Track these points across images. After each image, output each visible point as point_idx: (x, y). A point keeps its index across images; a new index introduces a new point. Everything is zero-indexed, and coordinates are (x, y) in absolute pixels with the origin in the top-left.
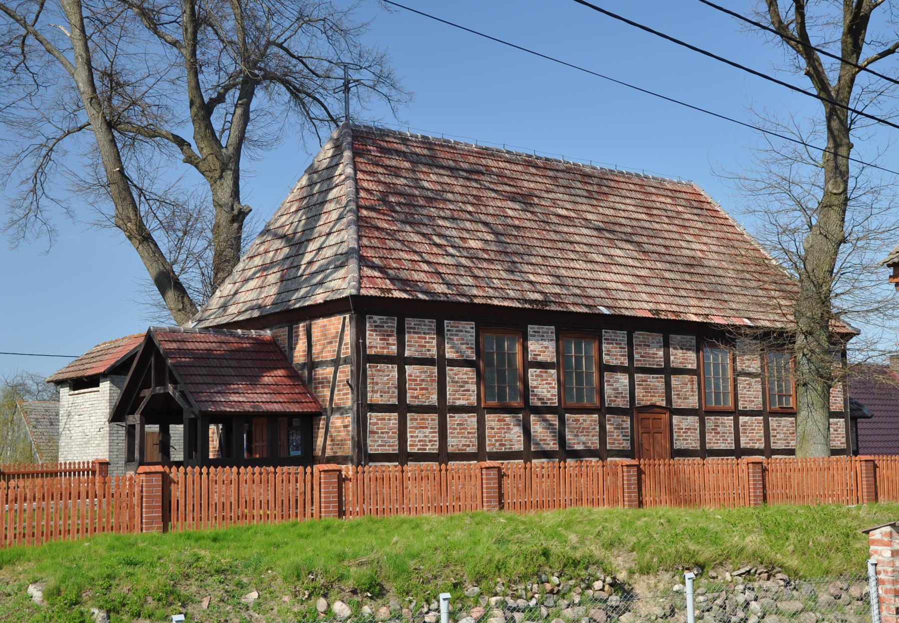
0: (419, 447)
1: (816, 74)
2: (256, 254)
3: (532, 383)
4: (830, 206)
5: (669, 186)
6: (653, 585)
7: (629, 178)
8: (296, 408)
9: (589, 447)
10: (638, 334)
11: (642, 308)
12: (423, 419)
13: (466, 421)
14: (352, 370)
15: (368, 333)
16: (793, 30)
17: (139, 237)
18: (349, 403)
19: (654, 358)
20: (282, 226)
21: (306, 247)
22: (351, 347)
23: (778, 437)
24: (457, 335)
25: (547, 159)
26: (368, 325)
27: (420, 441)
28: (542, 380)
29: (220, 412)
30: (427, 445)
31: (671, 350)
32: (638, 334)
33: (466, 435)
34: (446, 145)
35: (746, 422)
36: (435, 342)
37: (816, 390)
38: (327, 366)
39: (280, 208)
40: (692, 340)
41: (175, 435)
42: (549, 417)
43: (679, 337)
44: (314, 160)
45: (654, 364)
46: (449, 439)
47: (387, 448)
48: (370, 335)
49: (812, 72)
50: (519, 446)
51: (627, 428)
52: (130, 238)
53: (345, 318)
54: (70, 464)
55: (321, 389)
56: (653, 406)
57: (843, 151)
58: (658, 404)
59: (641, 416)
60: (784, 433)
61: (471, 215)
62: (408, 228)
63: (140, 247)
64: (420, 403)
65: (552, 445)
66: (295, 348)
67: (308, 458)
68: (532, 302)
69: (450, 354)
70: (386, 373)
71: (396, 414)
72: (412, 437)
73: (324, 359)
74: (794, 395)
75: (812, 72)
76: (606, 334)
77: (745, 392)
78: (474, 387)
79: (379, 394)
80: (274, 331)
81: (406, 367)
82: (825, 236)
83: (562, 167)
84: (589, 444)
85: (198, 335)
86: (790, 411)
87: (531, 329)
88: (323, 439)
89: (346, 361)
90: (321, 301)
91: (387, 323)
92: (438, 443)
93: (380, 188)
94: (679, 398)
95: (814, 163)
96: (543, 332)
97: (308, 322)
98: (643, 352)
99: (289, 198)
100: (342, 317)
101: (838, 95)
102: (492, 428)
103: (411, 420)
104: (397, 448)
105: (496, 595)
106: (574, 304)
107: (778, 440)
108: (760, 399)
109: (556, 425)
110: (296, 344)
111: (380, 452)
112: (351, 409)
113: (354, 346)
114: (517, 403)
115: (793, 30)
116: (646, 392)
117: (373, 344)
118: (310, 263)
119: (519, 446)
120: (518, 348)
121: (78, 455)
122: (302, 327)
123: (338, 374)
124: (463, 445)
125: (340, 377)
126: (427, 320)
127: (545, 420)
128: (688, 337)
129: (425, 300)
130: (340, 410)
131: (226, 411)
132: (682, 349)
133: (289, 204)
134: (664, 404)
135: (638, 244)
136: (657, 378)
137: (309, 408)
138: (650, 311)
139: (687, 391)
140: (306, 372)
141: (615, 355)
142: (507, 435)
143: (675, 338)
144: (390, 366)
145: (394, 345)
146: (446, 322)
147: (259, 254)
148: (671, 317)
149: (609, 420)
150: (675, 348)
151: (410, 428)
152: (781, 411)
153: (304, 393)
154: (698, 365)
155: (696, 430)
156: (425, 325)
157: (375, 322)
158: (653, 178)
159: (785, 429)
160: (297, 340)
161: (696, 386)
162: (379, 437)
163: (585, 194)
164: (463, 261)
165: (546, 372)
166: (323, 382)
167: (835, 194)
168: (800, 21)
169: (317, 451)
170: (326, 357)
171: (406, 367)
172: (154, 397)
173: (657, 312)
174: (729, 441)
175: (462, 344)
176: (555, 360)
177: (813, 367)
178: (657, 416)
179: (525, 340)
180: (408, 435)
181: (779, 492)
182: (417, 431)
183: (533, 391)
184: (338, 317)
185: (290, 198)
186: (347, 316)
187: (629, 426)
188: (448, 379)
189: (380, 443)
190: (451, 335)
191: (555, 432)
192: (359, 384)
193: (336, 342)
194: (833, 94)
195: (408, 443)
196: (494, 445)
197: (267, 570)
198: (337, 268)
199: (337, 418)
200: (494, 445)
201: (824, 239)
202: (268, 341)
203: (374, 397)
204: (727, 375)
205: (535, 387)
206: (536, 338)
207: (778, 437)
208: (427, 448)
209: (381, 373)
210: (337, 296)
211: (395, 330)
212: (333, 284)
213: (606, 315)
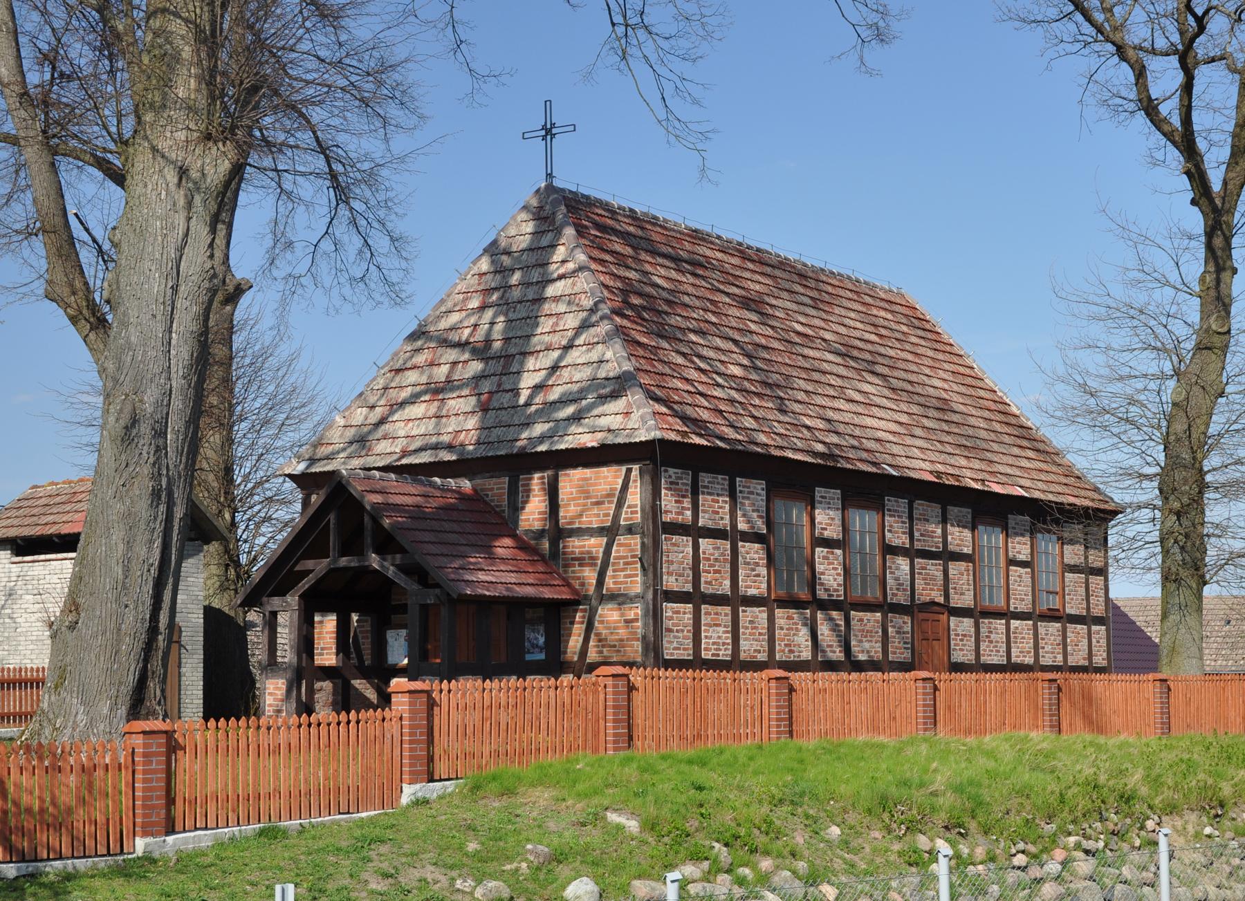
0: (713, 652)
1: (1197, 176)
2: (409, 365)
3: (819, 568)
4: (1209, 349)
5: (883, 295)
6: (1180, 828)
7: (841, 281)
8: (547, 593)
9: (872, 657)
10: (919, 504)
11: (921, 467)
12: (717, 614)
13: (757, 617)
14: (643, 544)
15: (663, 492)
16: (1170, 110)
17: (92, 320)
18: (638, 589)
19: (933, 537)
20: (453, 329)
21: (522, 363)
22: (643, 510)
23: (1046, 649)
24: (748, 498)
25: (758, 250)
26: (663, 480)
27: (714, 643)
28: (829, 564)
29: (476, 595)
30: (720, 650)
31: (949, 526)
32: (919, 504)
33: (757, 637)
34: (654, 221)
35: (1017, 628)
36: (727, 506)
37: (1191, 588)
38: (592, 536)
39: (442, 301)
40: (967, 512)
41: (188, 629)
42: (835, 614)
43: (956, 509)
44: (499, 234)
45: (932, 547)
46: (741, 642)
47: (682, 652)
48: (666, 495)
49: (1193, 170)
50: (806, 655)
51: (908, 633)
52: (74, 320)
53: (629, 471)
54: (38, 670)
55: (577, 568)
56: (933, 603)
57: (1225, 276)
58: (936, 600)
59: (921, 616)
60: (1052, 644)
61: (776, 332)
62: (665, 345)
63: (92, 336)
64: (714, 592)
65: (837, 655)
66: (523, 508)
67: (554, 665)
68: (816, 454)
69: (742, 526)
70: (681, 549)
71: (691, 605)
72: (706, 637)
73: (583, 526)
74: (1061, 593)
75: (1193, 170)
76: (890, 502)
77: (1016, 587)
78: (764, 571)
79: (674, 578)
80: (479, 481)
81: (700, 540)
82: (1203, 388)
83: (774, 261)
84: (872, 654)
85: (395, 483)
86: (1057, 614)
87: (819, 492)
88: (581, 639)
89: (630, 530)
90: (595, 444)
91: (681, 479)
92: (730, 647)
93: (619, 285)
94: (956, 593)
95: (1185, 289)
96: (830, 498)
97: (550, 472)
98: (922, 528)
99: (459, 287)
100: (624, 469)
101: (1223, 203)
102: (782, 628)
103: (706, 614)
104: (691, 652)
105: (1070, 834)
106: (861, 460)
107: (1046, 652)
108: (1030, 597)
109: (841, 625)
110: (526, 502)
111: (675, 657)
112: (642, 597)
113: (648, 508)
114: (804, 595)
115: (1170, 110)
116: (926, 584)
117: (669, 508)
118: (538, 388)
119: (806, 655)
120: (805, 519)
121: (33, 657)
122: (537, 481)
123: (615, 548)
124: (755, 651)
125: (618, 551)
126: (720, 477)
127: (831, 619)
128: (965, 510)
129: (725, 449)
130: (619, 598)
131: (485, 595)
132: (959, 526)
133: (461, 296)
134: (941, 600)
135: (884, 377)
136: (936, 565)
137: (565, 595)
138: (931, 472)
139: (963, 584)
140: (546, 545)
141: (897, 532)
142: (796, 638)
143: (953, 511)
144: (685, 538)
145: (688, 509)
146: (738, 479)
147: (414, 367)
148: (952, 482)
149: (892, 621)
150: (952, 525)
151: (705, 625)
152: (1049, 613)
153: (551, 573)
154: (974, 549)
155: (971, 636)
156: (718, 483)
157: (670, 477)
158: (866, 283)
159: (1052, 638)
160: (528, 496)
161: (971, 578)
162: (675, 637)
163: (809, 301)
164: (733, 393)
165: (833, 553)
166: (585, 560)
167: (1219, 333)
168: (1186, 104)
169: (569, 655)
170: (591, 522)
171: (700, 540)
172: (332, 572)
173: (938, 474)
174: (1001, 653)
175: (753, 511)
176: (841, 537)
177: (1187, 558)
178: (936, 617)
179: (813, 508)
180: (703, 634)
181: (748, 731)
182: (711, 629)
183: (820, 579)
184: (615, 468)
185: (462, 287)
186: (636, 468)
187: (909, 629)
188: (740, 558)
189: (675, 645)
190: (743, 498)
191: (840, 636)
192: (652, 563)
193: (610, 502)
194: (1218, 202)
195: (703, 646)
196: (783, 651)
197: (830, 799)
198: (603, 399)
199: (612, 610)
200: (783, 651)
201: (1201, 390)
202: (467, 495)
203: (671, 583)
204: (984, 562)
205: (823, 574)
206: (823, 505)
207: (1046, 649)
208: (721, 653)
209: (676, 548)
210: (620, 440)
211: (689, 488)
212: (604, 422)
213: (894, 476)
